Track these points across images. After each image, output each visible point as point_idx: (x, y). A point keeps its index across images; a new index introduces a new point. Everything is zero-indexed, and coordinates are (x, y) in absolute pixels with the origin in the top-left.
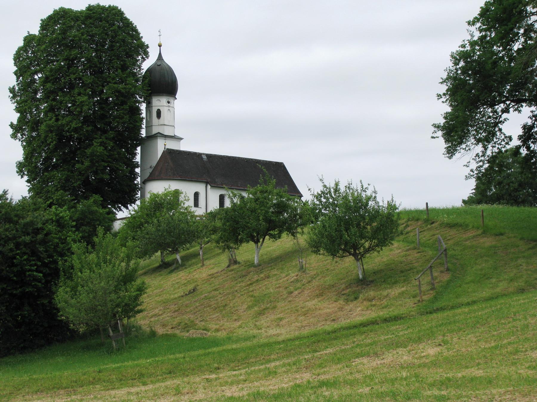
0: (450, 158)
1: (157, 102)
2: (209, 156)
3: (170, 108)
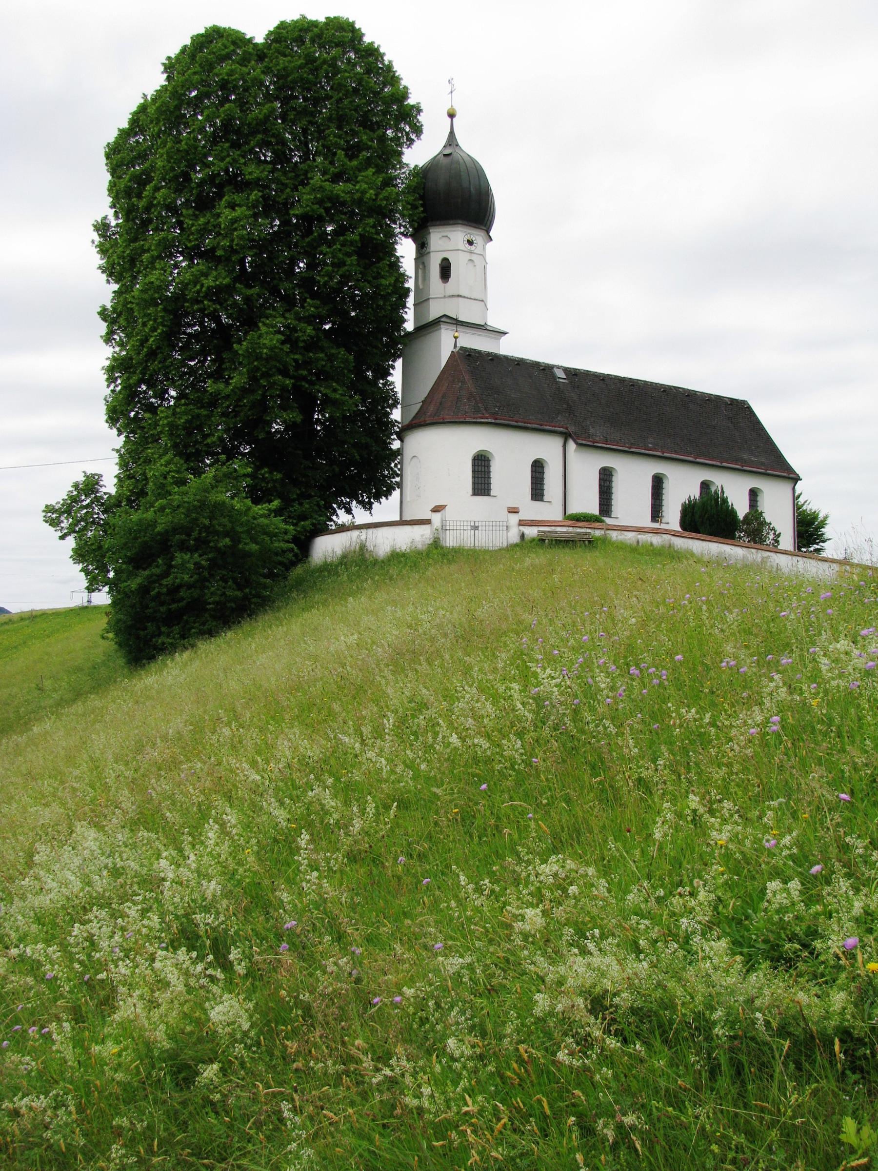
0: (53, 516)
1: (440, 242)
2: (572, 373)
3: (474, 257)
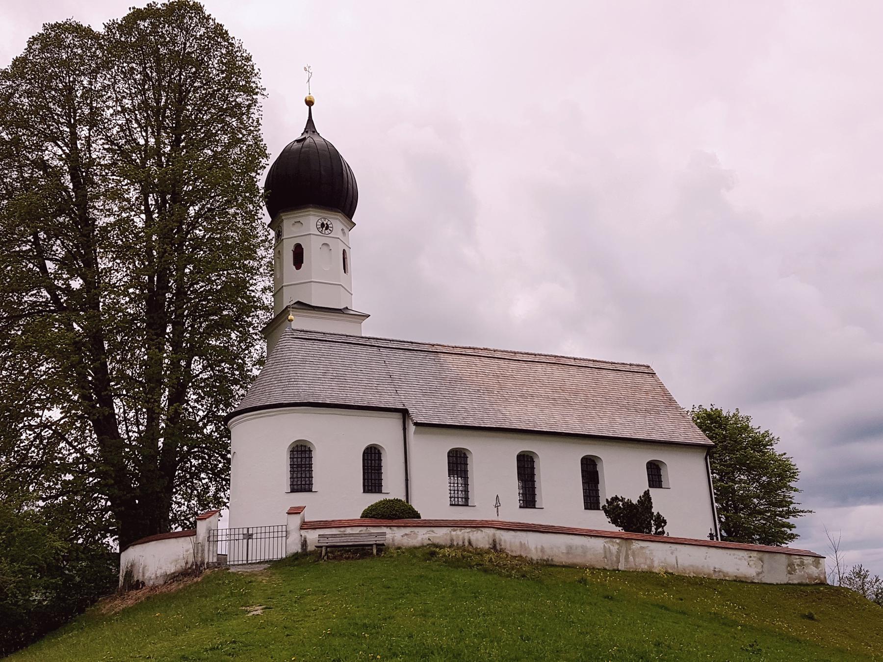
1: (294, 229)
